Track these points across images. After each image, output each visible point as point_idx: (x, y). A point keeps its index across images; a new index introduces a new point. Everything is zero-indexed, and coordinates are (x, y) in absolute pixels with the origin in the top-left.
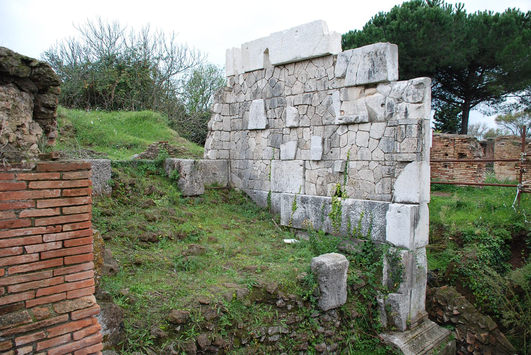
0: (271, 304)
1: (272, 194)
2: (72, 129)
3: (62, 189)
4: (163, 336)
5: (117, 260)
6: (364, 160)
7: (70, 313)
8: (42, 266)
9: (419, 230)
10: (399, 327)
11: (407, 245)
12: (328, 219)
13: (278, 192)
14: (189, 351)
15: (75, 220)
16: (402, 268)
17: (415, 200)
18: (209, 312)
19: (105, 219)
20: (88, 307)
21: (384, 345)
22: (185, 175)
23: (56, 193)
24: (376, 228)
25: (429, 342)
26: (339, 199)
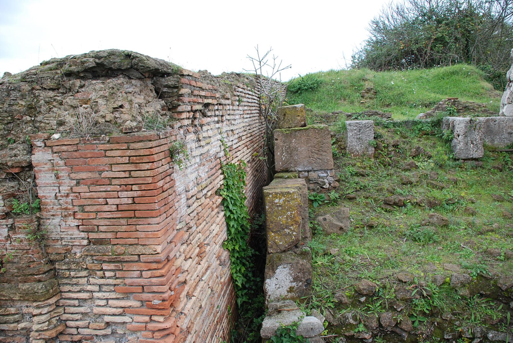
0: (503, 303)
2: (373, 90)
3: (130, 157)
4: (345, 302)
5: (352, 220)
7: (139, 255)
14: (367, 326)
15: (141, 182)
18: (403, 291)
19: (357, 179)
20: (152, 254)
22: (459, 136)
23: (125, 160)
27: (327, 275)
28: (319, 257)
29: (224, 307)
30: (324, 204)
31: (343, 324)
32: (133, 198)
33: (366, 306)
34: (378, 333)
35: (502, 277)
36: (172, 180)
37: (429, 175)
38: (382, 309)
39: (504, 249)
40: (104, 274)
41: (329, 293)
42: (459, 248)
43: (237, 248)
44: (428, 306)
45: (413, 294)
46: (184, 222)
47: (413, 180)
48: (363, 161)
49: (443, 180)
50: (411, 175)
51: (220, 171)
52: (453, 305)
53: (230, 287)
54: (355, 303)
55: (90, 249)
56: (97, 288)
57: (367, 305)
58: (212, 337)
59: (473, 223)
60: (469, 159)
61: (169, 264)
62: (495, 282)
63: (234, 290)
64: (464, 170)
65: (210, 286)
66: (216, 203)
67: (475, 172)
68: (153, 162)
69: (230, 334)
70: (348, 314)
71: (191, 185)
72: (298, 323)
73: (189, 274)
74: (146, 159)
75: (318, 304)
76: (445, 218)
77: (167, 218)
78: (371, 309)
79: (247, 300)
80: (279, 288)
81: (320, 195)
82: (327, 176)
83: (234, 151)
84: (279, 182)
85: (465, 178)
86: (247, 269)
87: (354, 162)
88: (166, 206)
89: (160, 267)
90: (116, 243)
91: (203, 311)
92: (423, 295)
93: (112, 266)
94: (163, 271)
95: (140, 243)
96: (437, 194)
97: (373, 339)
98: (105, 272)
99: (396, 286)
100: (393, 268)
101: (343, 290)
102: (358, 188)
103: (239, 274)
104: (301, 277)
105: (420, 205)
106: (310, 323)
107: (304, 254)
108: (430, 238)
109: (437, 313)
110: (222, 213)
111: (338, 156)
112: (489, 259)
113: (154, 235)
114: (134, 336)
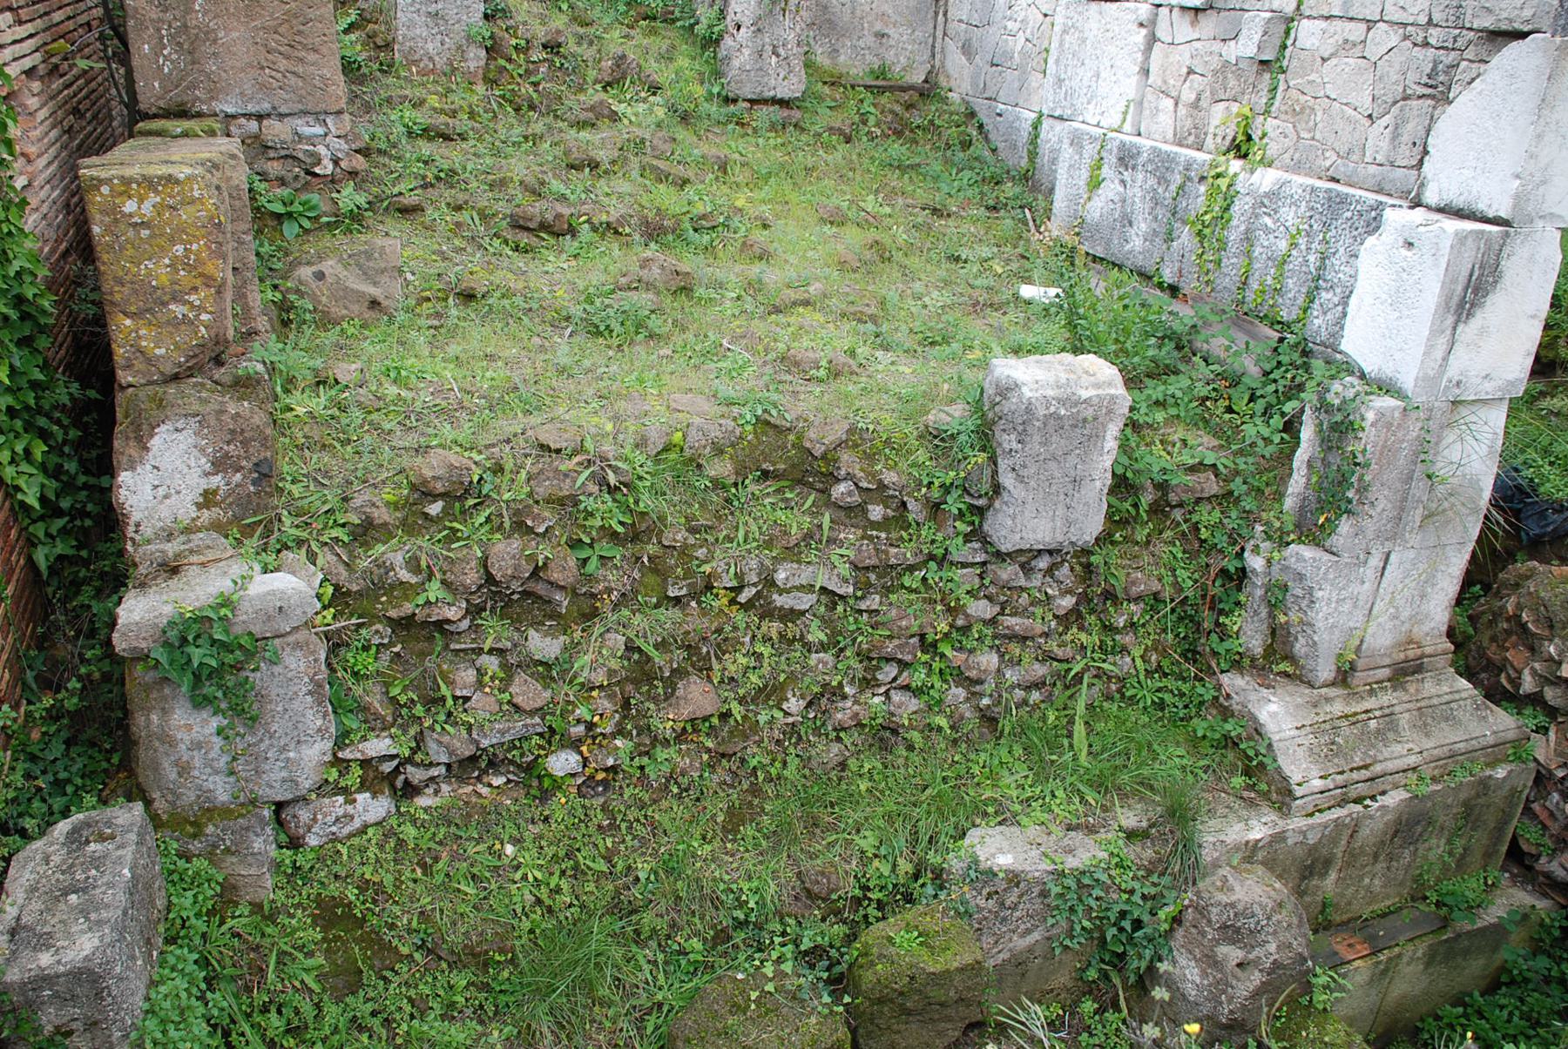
1: (1046, 124)
4: (381, 521)
5: (409, 276)
6: (1351, 19)
9: (1483, 331)
10: (1303, 667)
11: (1407, 382)
12: (1185, 238)
13: (1060, 118)
16: (1356, 464)
17: (1495, 207)
18: (551, 475)
19: (426, 148)
21: (1226, 713)
24: (1330, 295)
25: (1407, 746)
26: (1236, 165)
27: (324, 446)
28: (298, 394)
31: (381, 585)
34: (486, 602)
35: (816, 424)
37: (648, 143)
38: (492, 531)
41: (333, 500)
42: (717, 352)
44: (624, 513)
45: (579, 483)
47: (602, 155)
49: (688, 160)
50: (598, 143)
54: (413, 519)
57: (447, 524)
59: (760, 281)
60: (765, 102)
62: (798, 438)
63: (16, 520)
64: (750, 132)
67: (779, 140)
70: (394, 555)
72: (235, 597)
75: (299, 534)
76: (684, 267)
78: (459, 534)
79: (71, 552)
80: (166, 497)
81: (305, 197)
82: (326, 135)
85: (750, 156)
87: (419, 93)
92: (609, 485)
97: (471, 621)
99: (532, 464)
100: (528, 413)
101: (375, 486)
102: (430, 175)
103: (25, 467)
104: (238, 457)
105: (616, 232)
106: (272, 593)
107: (243, 385)
109: (649, 531)
111: (364, 70)
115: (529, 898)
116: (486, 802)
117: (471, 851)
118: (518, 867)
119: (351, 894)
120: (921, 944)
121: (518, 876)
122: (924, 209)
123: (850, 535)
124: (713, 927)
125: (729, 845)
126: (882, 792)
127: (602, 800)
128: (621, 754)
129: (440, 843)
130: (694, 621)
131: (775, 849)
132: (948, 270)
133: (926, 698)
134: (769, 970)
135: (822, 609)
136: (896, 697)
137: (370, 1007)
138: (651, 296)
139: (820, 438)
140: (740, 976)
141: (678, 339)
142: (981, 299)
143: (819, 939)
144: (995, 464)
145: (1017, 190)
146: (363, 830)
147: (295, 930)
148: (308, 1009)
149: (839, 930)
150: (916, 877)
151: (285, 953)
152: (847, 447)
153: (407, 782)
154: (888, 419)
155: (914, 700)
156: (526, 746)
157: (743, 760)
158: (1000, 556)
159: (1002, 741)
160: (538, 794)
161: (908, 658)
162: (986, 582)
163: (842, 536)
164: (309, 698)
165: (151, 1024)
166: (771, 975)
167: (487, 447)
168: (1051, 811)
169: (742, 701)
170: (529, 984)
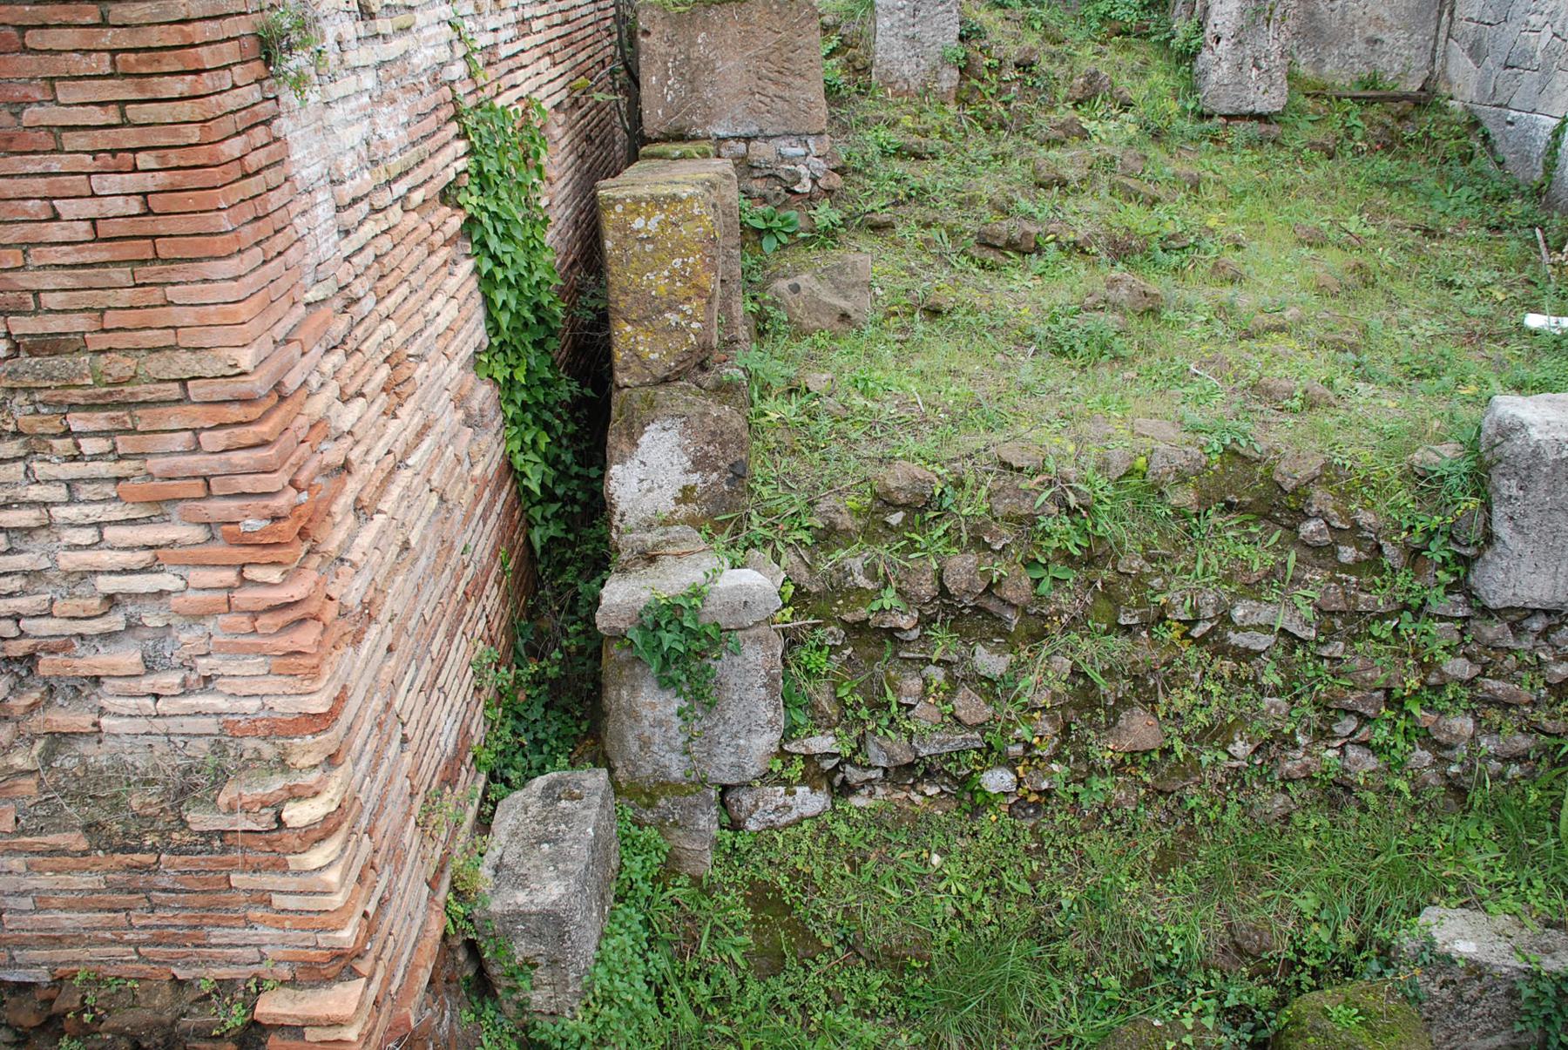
3: (114, 52)
5: (879, 291)
7: (183, 382)
8: (102, 253)
15: (164, 141)
18: (1011, 493)
19: (898, 167)
20: (223, 376)
29: (486, 553)
30: (797, 242)
31: (839, 589)
32: (145, 194)
33: (904, 538)
36: (276, 140)
38: (949, 544)
39: (1304, 380)
40: (78, 446)
41: (799, 502)
42: (1183, 377)
43: (520, 376)
45: (1038, 503)
46: (330, 282)
47: (1071, 174)
48: (922, 111)
50: (1067, 161)
51: (454, 128)
52: (1149, 533)
53: (504, 495)
54: (874, 528)
55: (21, 370)
56: (60, 493)
58: (450, 636)
59: (1232, 304)
61: (286, 407)
65: (435, 484)
66: (445, 228)
67: (1256, 157)
68: (197, 72)
69: (511, 629)
70: (853, 560)
71: (348, 163)
72: (706, 589)
73: (357, 442)
74: (171, 62)
76: (1152, 288)
77: (265, 262)
79: (560, 534)
80: (649, 490)
81: (783, 214)
83: (503, 68)
84: (651, 170)
86: (556, 441)
87: (893, 113)
88: (260, 223)
89: (253, 417)
90: (104, 347)
91: (417, 559)
92: (1068, 507)
93: (100, 421)
94: (264, 430)
95: (182, 344)
96: (1136, 217)
98: (81, 441)
100: (989, 429)
101: (839, 493)
103: (531, 456)
104: (717, 457)
105: (1083, 252)
106: (739, 588)
108: (1104, 347)
109: (1104, 556)
110: (467, 265)
111: (843, 93)
112: (1260, 407)
113: (225, 314)
114: (198, 630)
115: (950, 910)
116: (918, 810)
117: (899, 855)
118: (942, 878)
119: (783, 881)
120: (1361, 1023)
121: (942, 886)
122: (1414, 230)
123: (1317, 576)
124: (1133, 967)
125: (1158, 886)
126: (1328, 852)
127: (1032, 822)
128: (1057, 778)
129: (870, 844)
130: (1144, 652)
131: (1206, 896)
132: (1439, 297)
133: (1386, 757)
134: (1188, 1021)
135: (1280, 651)
136: (1353, 752)
137: (789, 991)
138: (1117, 317)
139: (1291, 472)
140: (1157, 1023)
141: (1143, 362)
142: (1477, 329)
143: (1245, 998)
144: (1489, 511)
145: (1528, 207)
146: (798, 822)
147: (727, 908)
148: (732, 983)
149: (1269, 992)
150: (1359, 948)
151: (717, 927)
152: (1320, 483)
153: (844, 781)
154: (1367, 456)
155: (1371, 758)
156: (963, 759)
157: (1181, 800)
158: (1487, 612)
159: (1470, 815)
160: (969, 808)
161: (1370, 712)
162: (1468, 639)
163: (1307, 576)
164: (763, 690)
165: (601, 971)
166: (1190, 1027)
167: (950, 461)
168: (1525, 901)
169: (1185, 738)
170: (942, 995)
